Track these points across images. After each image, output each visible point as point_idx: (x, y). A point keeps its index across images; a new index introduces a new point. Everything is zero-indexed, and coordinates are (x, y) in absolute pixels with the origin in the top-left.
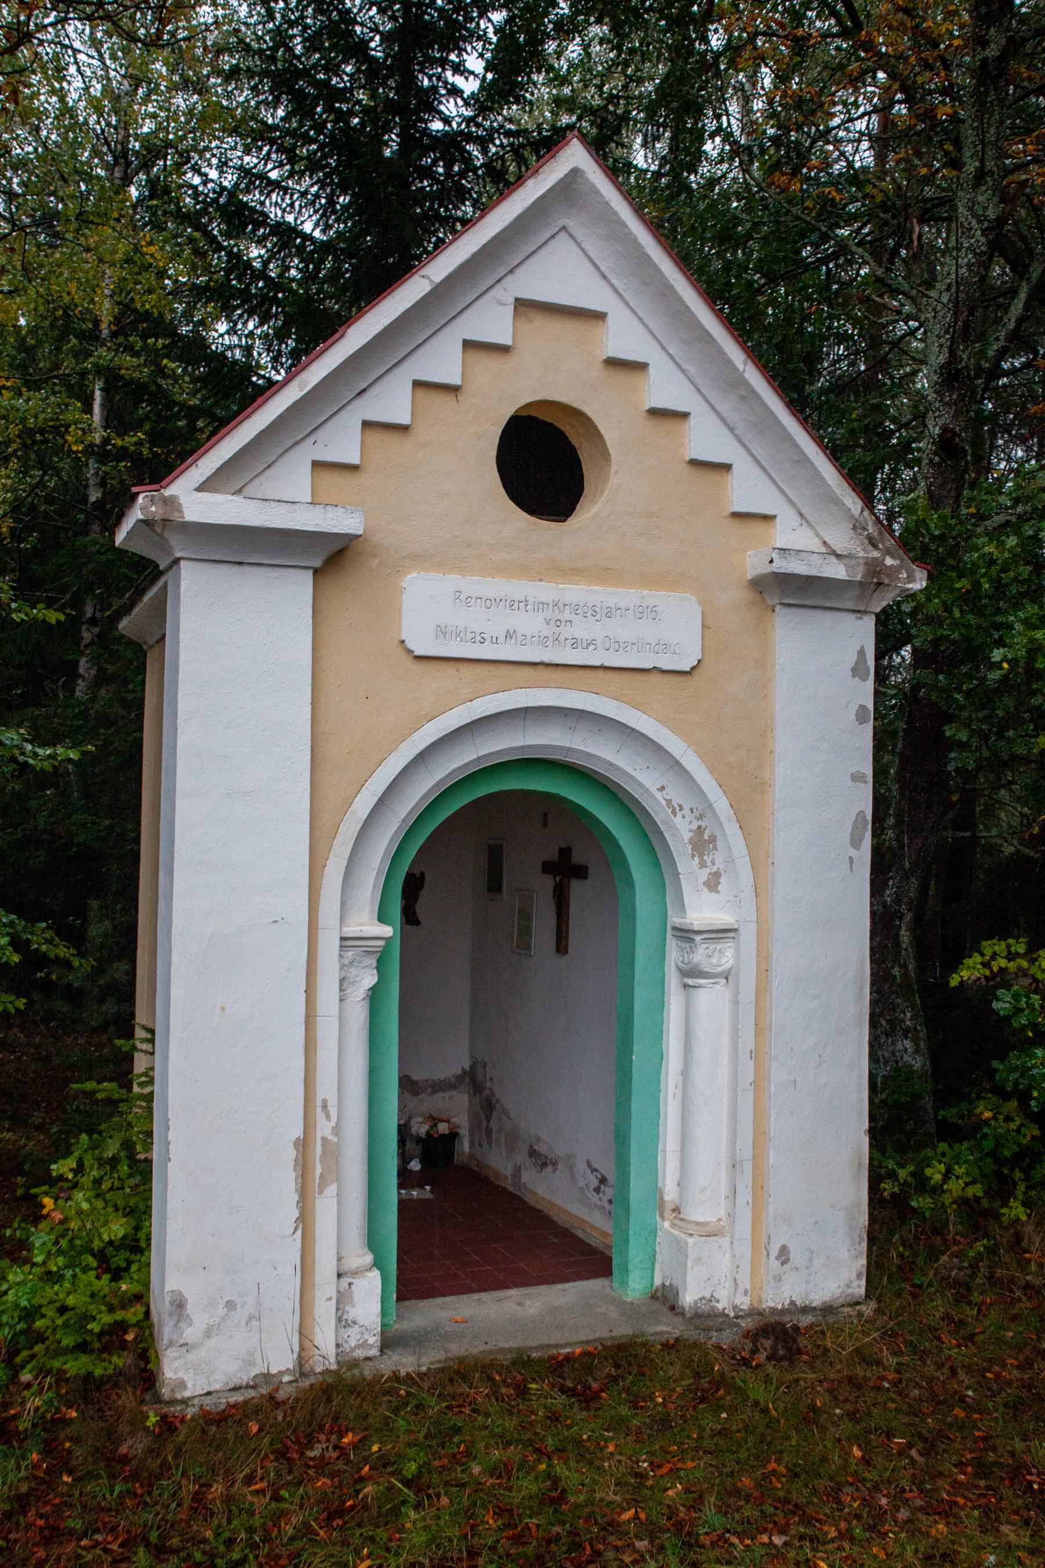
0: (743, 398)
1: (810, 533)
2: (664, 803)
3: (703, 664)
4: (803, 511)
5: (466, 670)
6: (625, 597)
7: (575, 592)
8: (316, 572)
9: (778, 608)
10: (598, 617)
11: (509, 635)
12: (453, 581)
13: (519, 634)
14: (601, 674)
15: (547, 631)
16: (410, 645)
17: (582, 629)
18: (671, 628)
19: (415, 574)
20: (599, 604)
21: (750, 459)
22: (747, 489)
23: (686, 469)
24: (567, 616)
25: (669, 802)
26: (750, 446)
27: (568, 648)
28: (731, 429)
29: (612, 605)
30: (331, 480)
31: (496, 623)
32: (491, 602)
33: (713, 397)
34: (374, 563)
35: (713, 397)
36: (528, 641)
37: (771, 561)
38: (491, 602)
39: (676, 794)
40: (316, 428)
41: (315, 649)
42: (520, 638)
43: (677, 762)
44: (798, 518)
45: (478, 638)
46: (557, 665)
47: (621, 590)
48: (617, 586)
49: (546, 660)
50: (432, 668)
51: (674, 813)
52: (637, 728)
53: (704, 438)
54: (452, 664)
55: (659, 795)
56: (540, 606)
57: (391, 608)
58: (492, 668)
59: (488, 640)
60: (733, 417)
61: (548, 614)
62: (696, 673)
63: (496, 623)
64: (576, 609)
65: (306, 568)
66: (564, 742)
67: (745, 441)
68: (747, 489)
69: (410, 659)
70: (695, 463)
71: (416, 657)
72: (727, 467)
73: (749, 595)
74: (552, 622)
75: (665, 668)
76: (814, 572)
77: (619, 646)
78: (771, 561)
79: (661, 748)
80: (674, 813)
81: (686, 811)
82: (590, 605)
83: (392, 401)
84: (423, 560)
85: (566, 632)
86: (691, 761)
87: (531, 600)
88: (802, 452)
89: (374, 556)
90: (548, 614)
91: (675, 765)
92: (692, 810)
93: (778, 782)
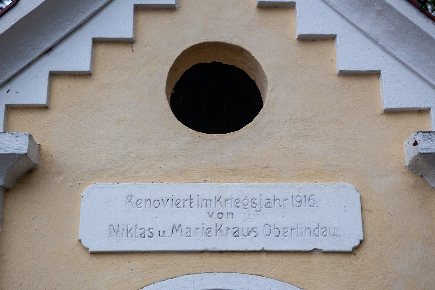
0: (380, 13)
3: (366, 244)
5: (137, 262)
6: (284, 189)
7: (234, 189)
10: (258, 208)
11: (174, 229)
12: (125, 188)
14: (264, 257)
15: (211, 223)
16: (84, 243)
17: (242, 219)
19: (92, 186)
21: (397, 64)
23: (338, 81)
24: (228, 209)
26: (394, 53)
28: (376, 42)
29: (271, 196)
31: (164, 219)
32: (157, 203)
33: (354, 18)
35: (354, 18)
36: (193, 234)
37: (416, 144)
42: (185, 231)
45: (147, 233)
46: (222, 252)
49: (210, 248)
53: (353, 51)
56: (203, 203)
60: (375, 32)
61: (211, 209)
62: (358, 253)
63: (164, 219)
67: (389, 49)
69: (88, 255)
70: (344, 74)
71: (93, 253)
72: (376, 74)
73: (409, 180)
74: (215, 215)
75: (326, 249)
77: (278, 232)
78: (416, 144)
82: (249, 198)
83: (76, 55)
84: (100, 173)
85: (228, 222)
87: (195, 197)
89: (60, 173)
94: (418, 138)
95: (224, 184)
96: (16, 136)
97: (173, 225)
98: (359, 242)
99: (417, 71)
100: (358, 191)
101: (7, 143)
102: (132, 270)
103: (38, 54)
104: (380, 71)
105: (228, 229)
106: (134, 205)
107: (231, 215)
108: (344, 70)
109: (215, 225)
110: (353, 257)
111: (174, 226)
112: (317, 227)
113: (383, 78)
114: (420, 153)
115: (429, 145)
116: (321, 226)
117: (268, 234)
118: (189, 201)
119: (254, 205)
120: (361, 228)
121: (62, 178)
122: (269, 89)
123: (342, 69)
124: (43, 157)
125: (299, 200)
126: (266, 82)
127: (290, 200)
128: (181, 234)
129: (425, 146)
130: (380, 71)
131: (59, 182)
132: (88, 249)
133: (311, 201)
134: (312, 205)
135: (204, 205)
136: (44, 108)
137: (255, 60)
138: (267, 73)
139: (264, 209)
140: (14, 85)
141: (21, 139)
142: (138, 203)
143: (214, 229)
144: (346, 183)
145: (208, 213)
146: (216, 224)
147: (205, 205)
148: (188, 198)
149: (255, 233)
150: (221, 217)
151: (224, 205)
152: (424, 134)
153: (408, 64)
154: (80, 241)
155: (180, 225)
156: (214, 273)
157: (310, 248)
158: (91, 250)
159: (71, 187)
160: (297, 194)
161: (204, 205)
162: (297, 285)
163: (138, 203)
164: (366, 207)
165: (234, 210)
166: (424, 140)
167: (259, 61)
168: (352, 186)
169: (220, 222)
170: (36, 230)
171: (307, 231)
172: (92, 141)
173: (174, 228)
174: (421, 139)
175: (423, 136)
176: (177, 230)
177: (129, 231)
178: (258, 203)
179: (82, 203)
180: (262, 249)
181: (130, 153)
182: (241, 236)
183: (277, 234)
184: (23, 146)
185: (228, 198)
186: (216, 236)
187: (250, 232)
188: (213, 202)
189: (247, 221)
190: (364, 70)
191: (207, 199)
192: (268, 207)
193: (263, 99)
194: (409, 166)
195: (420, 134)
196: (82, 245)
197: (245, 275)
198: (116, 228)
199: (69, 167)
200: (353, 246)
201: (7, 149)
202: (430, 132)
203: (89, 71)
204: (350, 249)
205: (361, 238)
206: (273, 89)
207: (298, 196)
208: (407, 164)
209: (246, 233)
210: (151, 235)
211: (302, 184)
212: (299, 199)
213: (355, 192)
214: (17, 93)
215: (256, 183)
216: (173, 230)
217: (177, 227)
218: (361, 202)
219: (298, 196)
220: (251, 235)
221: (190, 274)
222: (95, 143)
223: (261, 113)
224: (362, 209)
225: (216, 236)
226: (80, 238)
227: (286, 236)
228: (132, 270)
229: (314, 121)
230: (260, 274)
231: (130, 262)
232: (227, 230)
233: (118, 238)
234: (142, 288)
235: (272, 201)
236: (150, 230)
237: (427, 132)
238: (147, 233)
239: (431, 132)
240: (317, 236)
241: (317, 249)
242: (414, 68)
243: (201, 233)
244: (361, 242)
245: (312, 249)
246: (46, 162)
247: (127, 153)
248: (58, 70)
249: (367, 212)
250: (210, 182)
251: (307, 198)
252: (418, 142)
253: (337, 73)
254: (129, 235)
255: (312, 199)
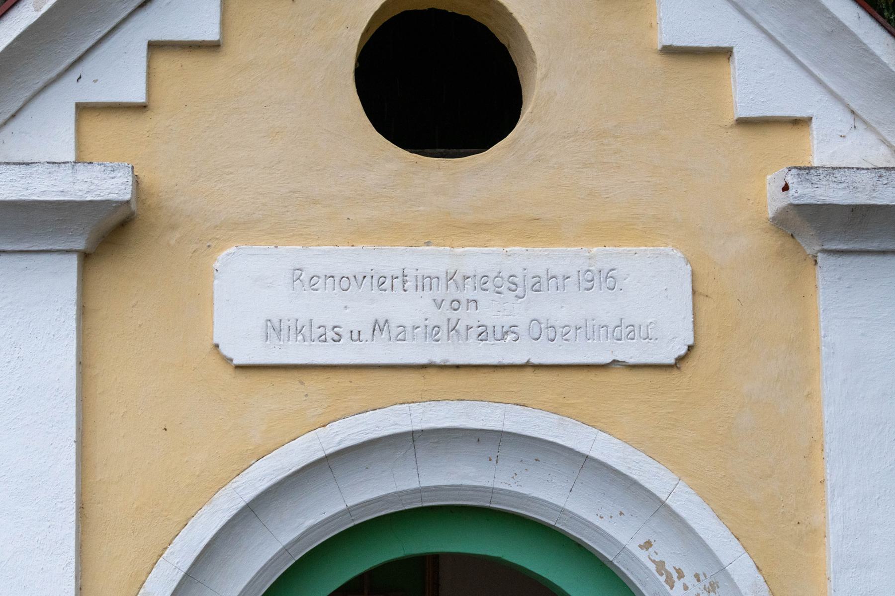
1: (871, 138)
2: (652, 567)
3: (696, 352)
4: (854, 107)
5: (315, 383)
6: (563, 259)
7: (479, 258)
8: (86, 257)
9: (820, 257)
10: (519, 292)
12: (290, 255)
13: (393, 325)
14: (528, 376)
15: (438, 317)
16: (225, 350)
17: (492, 311)
18: (646, 301)
19: (232, 250)
20: (518, 271)
21: (761, 36)
22: (760, 81)
23: (659, 62)
25: (660, 566)
26: (757, 17)
27: (473, 340)
29: (542, 272)
30: (102, 129)
31: (357, 311)
32: (346, 282)
34: (174, 237)
36: (409, 336)
37: (786, 188)
38: (346, 282)
39: (669, 553)
40: (80, 59)
41: (82, 365)
43: (663, 504)
44: (849, 117)
45: (330, 334)
46: (458, 367)
47: (558, 249)
48: (551, 244)
49: (438, 360)
50: (256, 377)
51: (670, 582)
52: (593, 454)
54: (296, 374)
55: (642, 555)
56: (426, 282)
57: (202, 299)
58: (355, 376)
59: (346, 336)
61: (440, 292)
62: (684, 366)
63: (357, 311)
64: (483, 282)
65: (68, 252)
66: (484, 481)
67: (748, 10)
68: (760, 81)
69: (230, 370)
74: (446, 304)
75: (632, 361)
76: (861, 199)
78: (786, 188)
79: (635, 483)
80: (670, 582)
81: (689, 579)
82: (505, 274)
84: (243, 229)
85: (468, 317)
86: (685, 502)
88: (834, 18)
89: (173, 227)
90: (440, 292)
91: (660, 508)
92: (697, 577)
93: (834, 530)
94: (790, 179)
95: (461, 250)
96: (110, 169)
97: (374, 321)
98: (686, 347)
99: (792, 51)
100: (688, 262)
101: (96, 182)
102: (306, 395)
103: (129, 10)
104: (732, 48)
105: (468, 328)
106: (307, 286)
107: (474, 304)
108: (670, 46)
109: (446, 322)
110: (675, 372)
111: (376, 322)
112: (619, 323)
113: (736, 62)
114: (791, 205)
115: (806, 191)
116: (626, 322)
117: (536, 337)
118: (399, 280)
119: (514, 287)
120: (691, 326)
121: (177, 235)
122: (539, 74)
123: (668, 43)
124: (144, 198)
125: (590, 279)
126: (533, 61)
127: (574, 279)
128: (388, 336)
129: (799, 192)
130: (732, 48)
131: (173, 242)
132: (231, 360)
133: (608, 279)
134: (611, 286)
135: (427, 288)
136: (141, 108)
137: (514, 20)
138: (536, 46)
139: (530, 294)
140: (87, 68)
141: (119, 175)
142: (313, 282)
143: (444, 328)
144: (669, 249)
145: (434, 300)
146: (449, 320)
147: (428, 287)
148: (400, 274)
149: (514, 335)
150: (456, 307)
151: (462, 287)
152: (799, 171)
153: (779, 39)
154: (217, 346)
155: (386, 321)
156: (444, 402)
157: (606, 359)
158: (236, 362)
159: (195, 251)
160: (587, 268)
161: (427, 288)
162: (584, 421)
163: (313, 282)
164: (700, 289)
165: (478, 295)
166: (799, 183)
167: (521, 21)
168: (679, 254)
169: (454, 316)
170: (140, 326)
171: (603, 331)
172: (227, 170)
173: (377, 326)
174: (795, 180)
175: (798, 174)
176: (381, 330)
177: (298, 331)
178: (520, 284)
179: (216, 282)
180: (525, 361)
181: (294, 192)
182: (491, 341)
183: (552, 336)
184: (123, 187)
185: (468, 275)
186: (448, 339)
187: (506, 332)
188: (443, 281)
189: (501, 314)
190: (705, 45)
191: (433, 275)
192: (536, 291)
193: (520, 74)
194: (774, 219)
195: (794, 171)
196: (219, 353)
197: (497, 405)
198: (277, 325)
199: (189, 216)
200: (676, 356)
201: (98, 193)
202: (809, 168)
203: (219, 41)
204: (671, 361)
205: (691, 342)
206: (545, 76)
207: (589, 271)
208: (770, 215)
209: (499, 336)
210: (337, 337)
211: (595, 249)
212: (589, 276)
213: (684, 263)
214: (95, 81)
215: (517, 248)
216: (374, 330)
217: (382, 325)
218: (693, 281)
219: (589, 271)
220: (508, 338)
221: (404, 403)
222: (231, 173)
223: (525, 121)
224: (694, 292)
225: (448, 339)
226: (216, 341)
227: (566, 340)
228: (306, 395)
229: (618, 137)
230: (522, 403)
231: (302, 383)
232: (468, 330)
233: (282, 343)
234: (324, 426)
235: (544, 280)
236: (336, 329)
237: (805, 168)
238: (330, 334)
239: (812, 168)
240: (618, 340)
241: (618, 361)
242: (789, 47)
243: (423, 335)
244: (690, 348)
245: (610, 361)
246: (149, 206)
247: (290, 192)
248: (163, 39)
249: (702, 297)
250: (436, 245)
251: (604, 274)
252: (790, 186)
253: (659, 47)
254: (300, 337)
255: (611, 277)
